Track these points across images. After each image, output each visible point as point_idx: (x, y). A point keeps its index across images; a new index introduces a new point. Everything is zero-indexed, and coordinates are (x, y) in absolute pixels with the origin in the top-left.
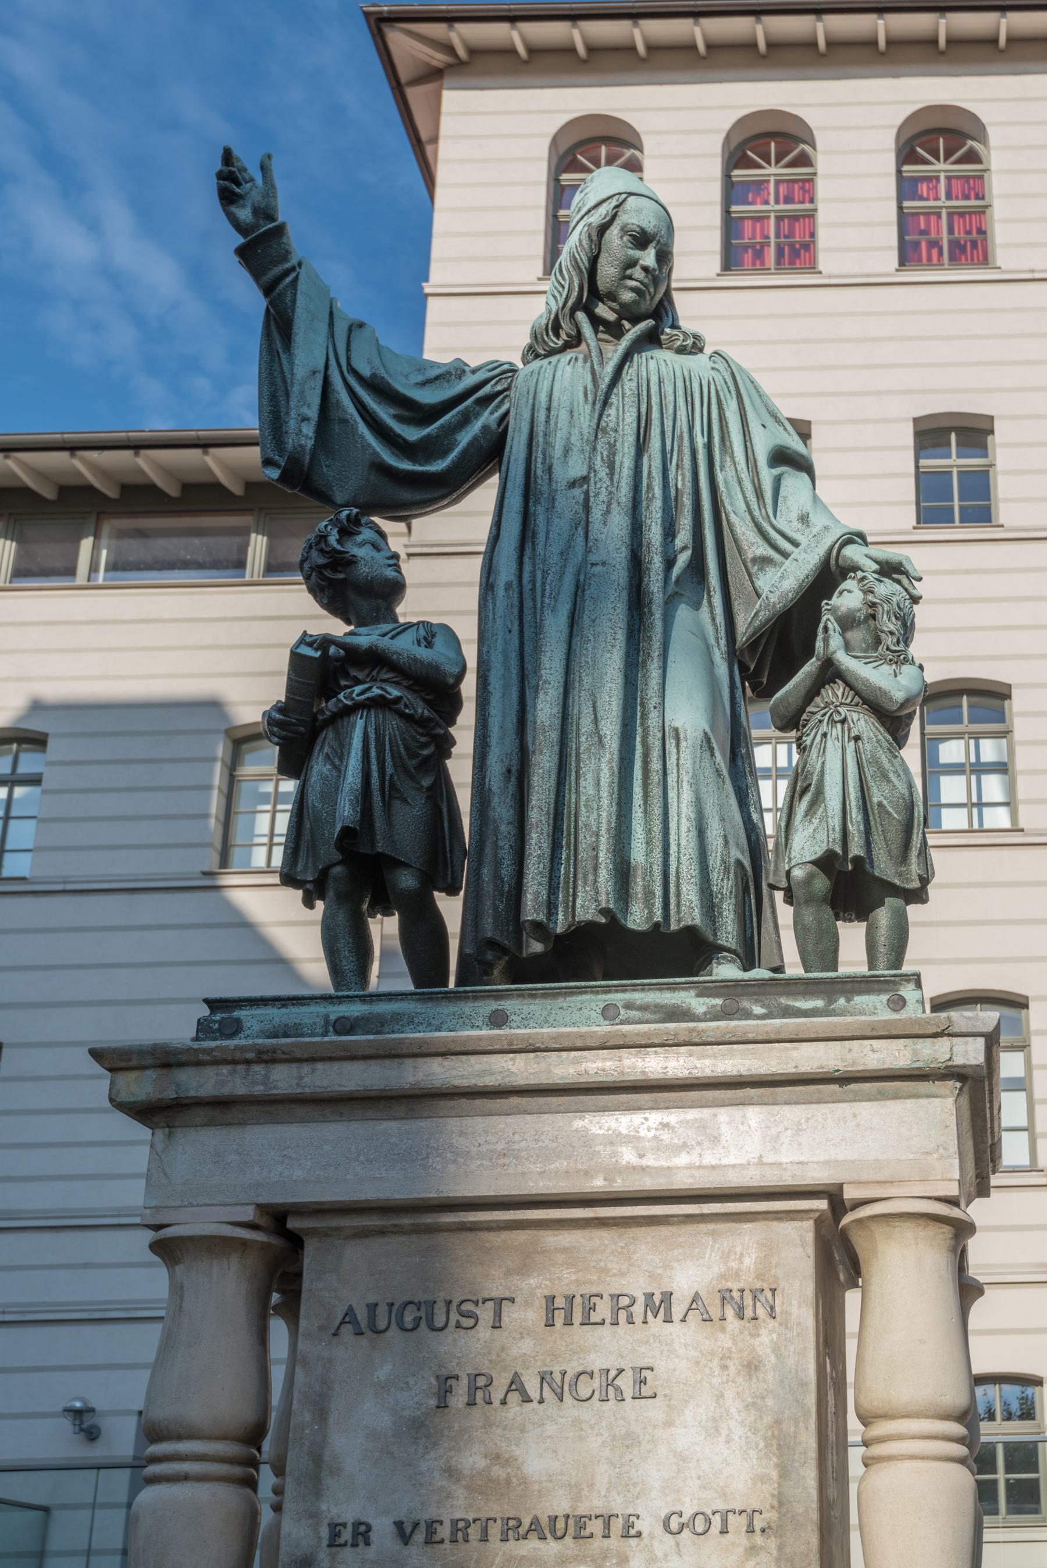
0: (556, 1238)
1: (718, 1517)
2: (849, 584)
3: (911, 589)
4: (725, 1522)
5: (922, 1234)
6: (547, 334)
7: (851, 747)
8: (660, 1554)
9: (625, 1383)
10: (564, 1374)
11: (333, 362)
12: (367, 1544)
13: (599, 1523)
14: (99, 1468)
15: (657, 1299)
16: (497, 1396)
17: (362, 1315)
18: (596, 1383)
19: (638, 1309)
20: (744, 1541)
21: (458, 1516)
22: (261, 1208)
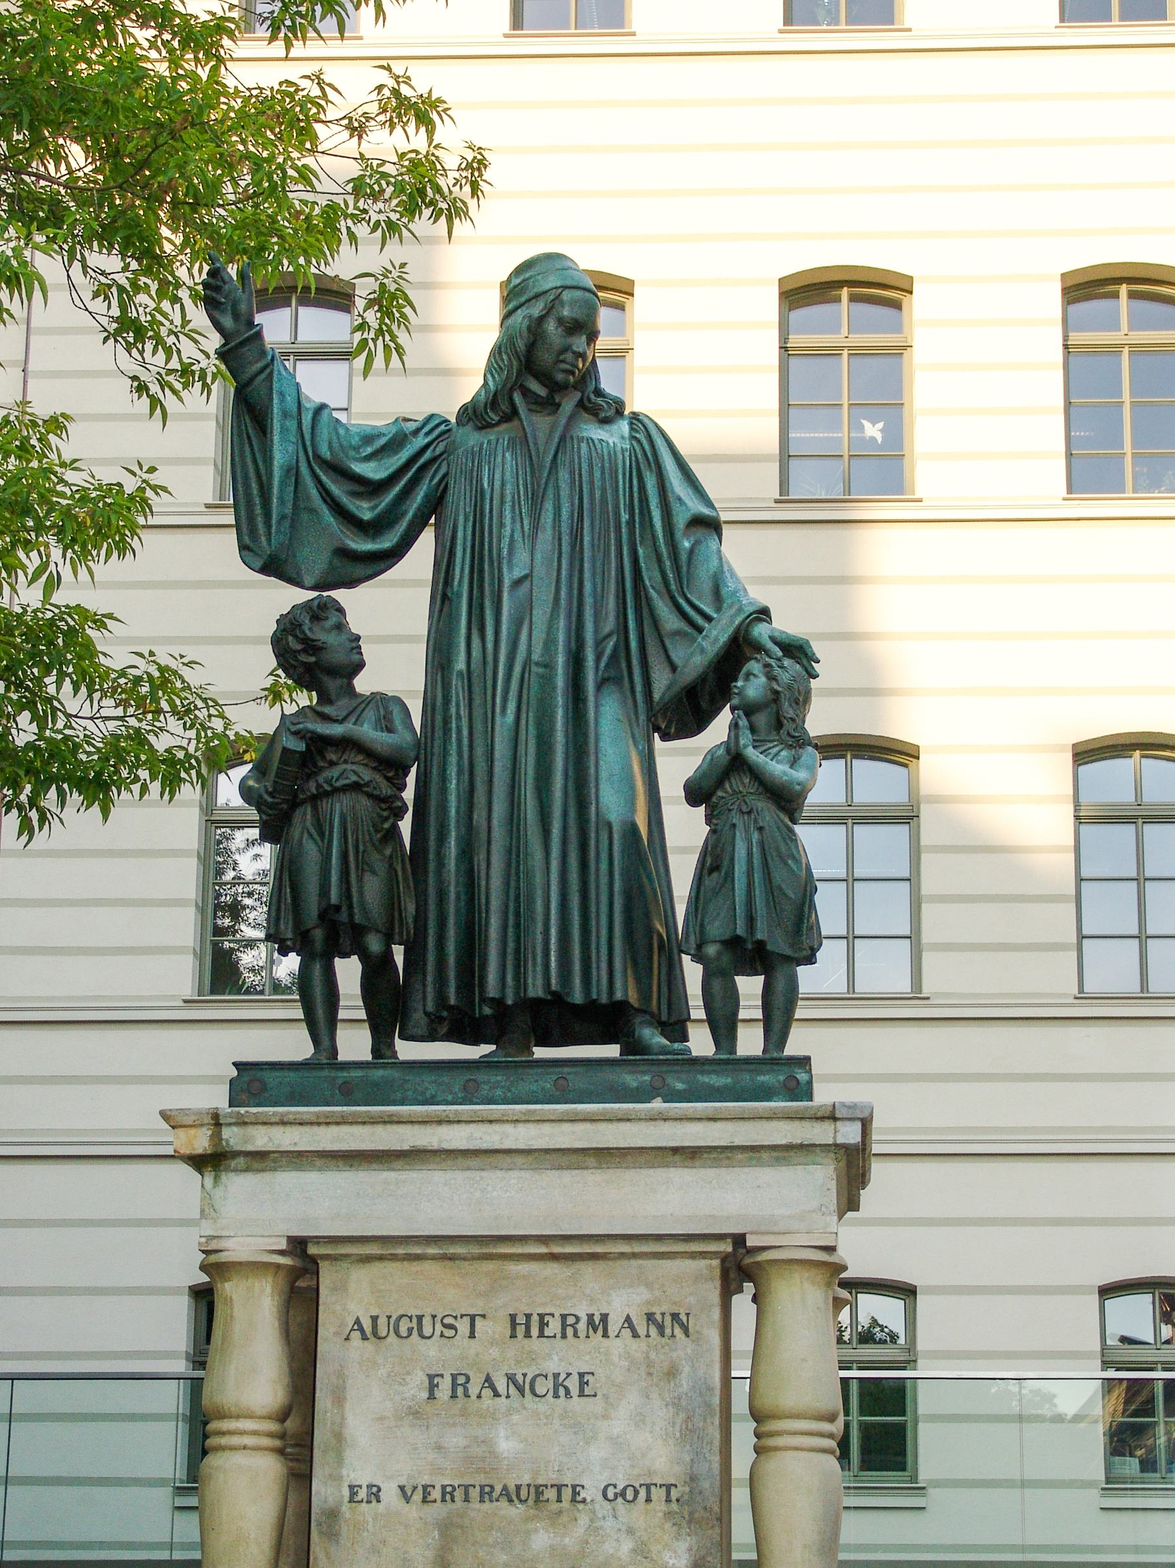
0: (516, 1268)
1: (644, 1488)
2: (754, 666)
3: (810, 669)
4: (648, 1492)
5: (806, 1275)
6: (487, 413)
7: (755, 836)
8: (600, 1516)
9: (573, 1384)
10: (525, 1375)
12: (379, 1501)
15: (597, 1319)
16: (474, 1390)
17: (367, 1325)
18: (550, 1383)
19: (582, 1326)
20: (663, 1507)
21: (446, 1483)
22: (291, 1239)
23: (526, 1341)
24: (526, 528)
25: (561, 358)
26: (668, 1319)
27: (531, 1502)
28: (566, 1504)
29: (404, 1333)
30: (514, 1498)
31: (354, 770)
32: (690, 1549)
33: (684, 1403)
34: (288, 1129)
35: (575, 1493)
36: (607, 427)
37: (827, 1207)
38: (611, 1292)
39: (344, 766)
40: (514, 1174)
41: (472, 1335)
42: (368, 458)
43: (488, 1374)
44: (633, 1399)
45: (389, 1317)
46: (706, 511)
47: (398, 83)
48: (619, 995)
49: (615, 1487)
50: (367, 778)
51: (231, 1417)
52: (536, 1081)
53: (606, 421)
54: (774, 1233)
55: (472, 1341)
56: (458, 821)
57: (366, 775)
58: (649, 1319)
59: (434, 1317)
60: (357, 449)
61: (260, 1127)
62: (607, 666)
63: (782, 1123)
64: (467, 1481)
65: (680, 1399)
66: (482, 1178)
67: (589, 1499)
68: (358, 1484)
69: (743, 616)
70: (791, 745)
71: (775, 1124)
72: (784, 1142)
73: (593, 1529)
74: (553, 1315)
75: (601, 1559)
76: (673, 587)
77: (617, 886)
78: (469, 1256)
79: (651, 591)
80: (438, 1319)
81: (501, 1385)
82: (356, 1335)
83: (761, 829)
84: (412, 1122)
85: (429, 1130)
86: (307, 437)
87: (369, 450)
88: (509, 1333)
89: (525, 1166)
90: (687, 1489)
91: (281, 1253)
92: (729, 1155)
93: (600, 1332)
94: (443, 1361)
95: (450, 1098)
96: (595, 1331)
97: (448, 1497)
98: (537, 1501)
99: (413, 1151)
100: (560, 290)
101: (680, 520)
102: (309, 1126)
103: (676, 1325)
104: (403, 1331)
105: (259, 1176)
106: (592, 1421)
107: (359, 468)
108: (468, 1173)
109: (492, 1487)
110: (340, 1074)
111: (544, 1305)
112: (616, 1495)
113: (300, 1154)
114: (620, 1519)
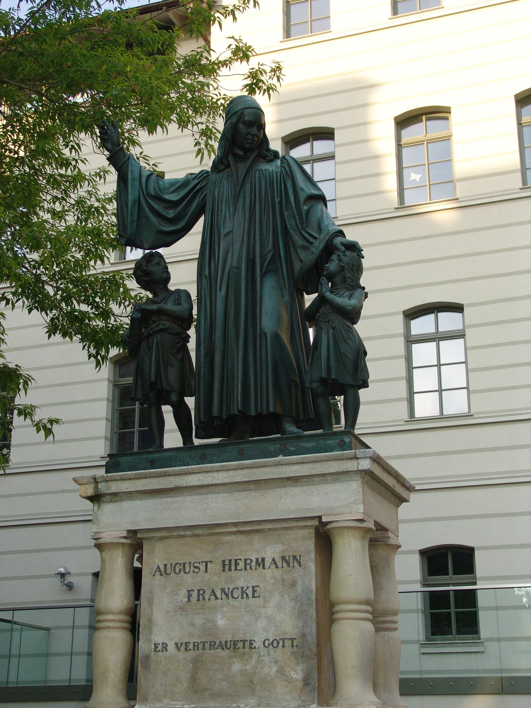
1: (281, 640)
2: (334, 257)
6: (218, 165)
8: (262, 654)
9: (250, 592)
10: (229, 588)
11: (141, 195)
12: (166, 651)
13: (242, 643)
14: (75, 607)
15: (260, 560)
16: (207, 597)
17: (162, 568)
18: (240, 592)
21: (195, 641)
22: (129, 531)
23: (229, 572)
24: (231, 211)
25: (247, 138)
26: (291, 558)
27: (232, 649)
28: (247, 649)
29: (177, 571)
30: (224, 647)
31: (166, 323)
32: (303, 670)
33: (299, 598)
34: (125, 482)
35: (251, 644)
36: (270, 164)
37: (358, 501)
38: (266, 547)
39: (159, 322)
40: (220, 495)
41: (206, 571)
42: (173, 192)
43: (213, 589)
44: (276, 597)
45: (171, 564)
46: (315, 192)
47: (238, 43)
48: (272, 409)
49: (269, 641)
50: (167, 326)
51: (103, 614)
52: (231, 452)
53: (271, 161)
54: (334, 515)
55: (206, 573)
56: (204, 340)
57: (167, 324)
58: (283, 559)
59: (190, 563)
60: (168, 189)
61: (113, 482)
62: (269, 264)
63: (333, 462)
64: (204, 640)
65: (297, 597)
66: (207, 498)
67: (257, 647)
68: (158, 643)
69: (329, 235)
70: (349, 289)
71: (330, 463)
72: (334, 471)
73: (259, 661)
74: (241, 559)
75: (263, 675)
76: (300, 227)
77: (270, 360)
78: (205, 534)
79: (290, 230)
80: (192, 564)
81: (219, 594)
82: (158, 573)
83: (334, 328)
84: (174, 475)
85: (182, 478)
86: (144, 187)
87: (173, 189)
88: (222, 569)
89: (225, 491)
90: (301, 640)
91: (125, 538)
92: (312, 479)
93: (261, 566)
94: (194, 583)
95: (194, 463)
96: (259, 566)
97: (196, 648)
98: (234, 648)
99: (175, 488)
100: (243, 110)
101: (302, 197)
102: (133, 480)
103: (295, 561)
104: (177, 570)
105: (116, 504)
106: (258, 609)
107: (167, 197)
108: (201, 496)
109: (215, 642)
110: (150, 456)
111: (237, 555)
112: (269, 644)
113: (131, 492)
114: (271, 656)
